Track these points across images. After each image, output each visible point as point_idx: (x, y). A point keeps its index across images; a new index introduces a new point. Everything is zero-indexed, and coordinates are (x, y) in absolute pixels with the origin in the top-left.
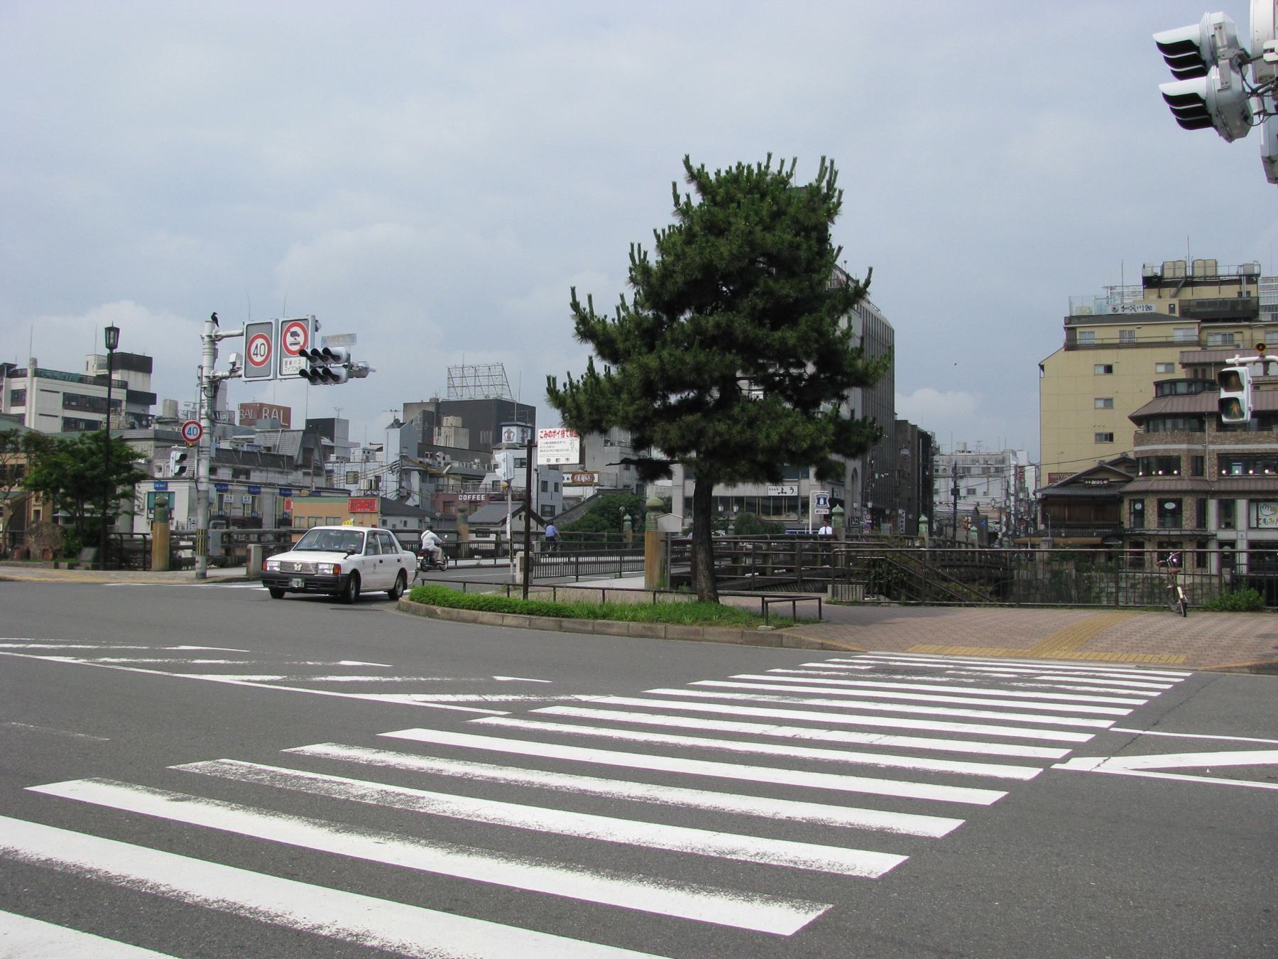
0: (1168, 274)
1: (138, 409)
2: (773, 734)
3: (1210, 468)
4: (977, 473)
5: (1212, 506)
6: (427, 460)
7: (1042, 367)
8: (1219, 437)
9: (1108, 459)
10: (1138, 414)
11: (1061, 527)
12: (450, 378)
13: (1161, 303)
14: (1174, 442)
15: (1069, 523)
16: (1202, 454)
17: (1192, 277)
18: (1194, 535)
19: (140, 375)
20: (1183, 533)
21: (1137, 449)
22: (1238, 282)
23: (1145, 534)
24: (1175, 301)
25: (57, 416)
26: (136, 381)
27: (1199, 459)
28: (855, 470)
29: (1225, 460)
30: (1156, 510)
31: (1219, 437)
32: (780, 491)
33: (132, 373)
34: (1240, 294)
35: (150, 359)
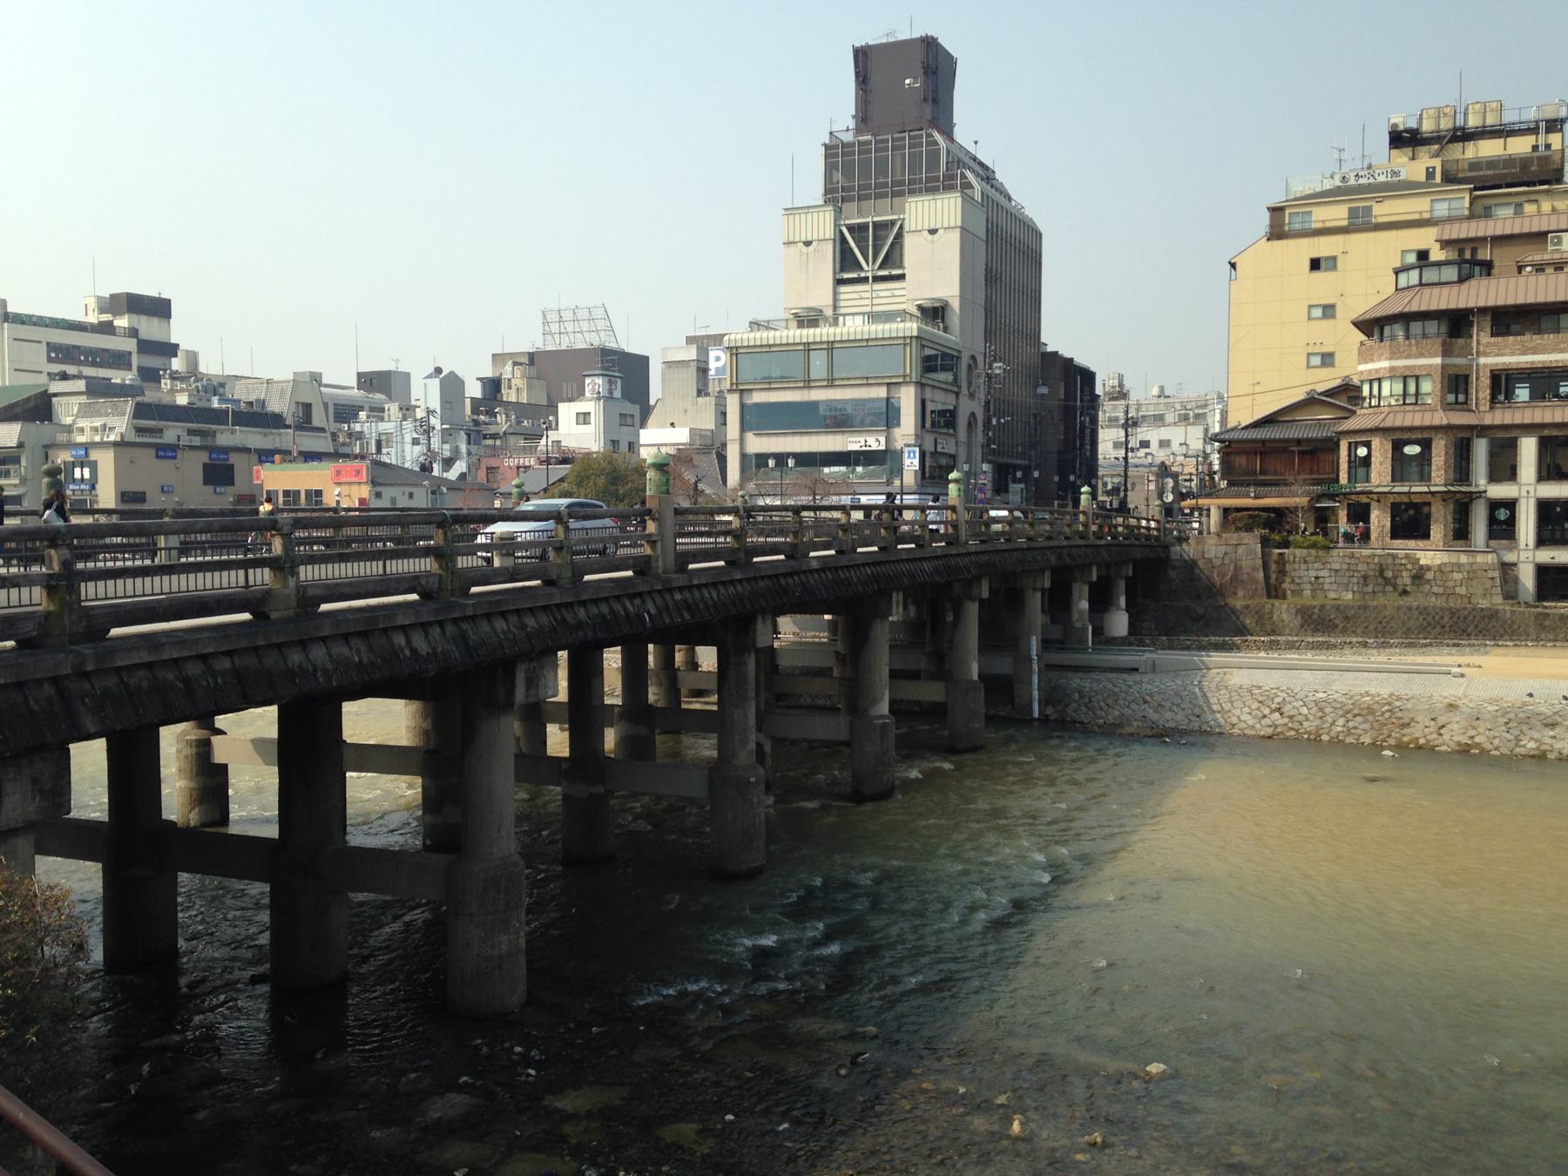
0: (1427, 127)
1: (152, 362)
2: (106, 782)
3: (1481, 390)
4: (1172, 420)
5: (1481, 449)
6: (482, 418)
7: (1233, 266)
8: (1495, 344)
9: (1321, 388)
10: (1367, 317)
11: (1249, 485)
12: (546, 322)
13: (1414, 166)
14: (1422, 355)
15: (1262, 477)
16: (1467, 372)
17: (1463, 129)
18: (1449, 492)
19: (155, 321)
20: (1433, 489)
21: (1362, 367)
22: (1533, 131)
23: (1371, 493)
24: (1437, 163)
25: (41, 372)
26: (150, 328)
27: (1461, 380)
28: (973, 414)
29: (1502, 383)
30: (1390, 456)
31: (1495, 344)
32: (863, 443)
33: (144, 319)
34: (1535, 148)
35: (168, 302)
